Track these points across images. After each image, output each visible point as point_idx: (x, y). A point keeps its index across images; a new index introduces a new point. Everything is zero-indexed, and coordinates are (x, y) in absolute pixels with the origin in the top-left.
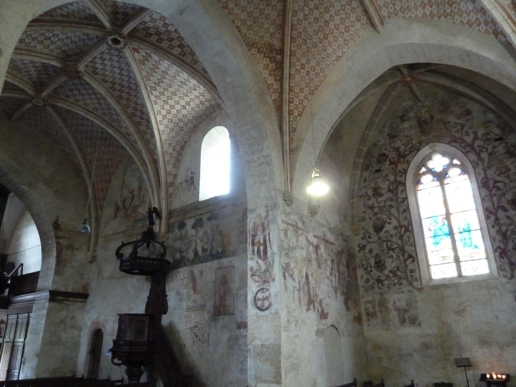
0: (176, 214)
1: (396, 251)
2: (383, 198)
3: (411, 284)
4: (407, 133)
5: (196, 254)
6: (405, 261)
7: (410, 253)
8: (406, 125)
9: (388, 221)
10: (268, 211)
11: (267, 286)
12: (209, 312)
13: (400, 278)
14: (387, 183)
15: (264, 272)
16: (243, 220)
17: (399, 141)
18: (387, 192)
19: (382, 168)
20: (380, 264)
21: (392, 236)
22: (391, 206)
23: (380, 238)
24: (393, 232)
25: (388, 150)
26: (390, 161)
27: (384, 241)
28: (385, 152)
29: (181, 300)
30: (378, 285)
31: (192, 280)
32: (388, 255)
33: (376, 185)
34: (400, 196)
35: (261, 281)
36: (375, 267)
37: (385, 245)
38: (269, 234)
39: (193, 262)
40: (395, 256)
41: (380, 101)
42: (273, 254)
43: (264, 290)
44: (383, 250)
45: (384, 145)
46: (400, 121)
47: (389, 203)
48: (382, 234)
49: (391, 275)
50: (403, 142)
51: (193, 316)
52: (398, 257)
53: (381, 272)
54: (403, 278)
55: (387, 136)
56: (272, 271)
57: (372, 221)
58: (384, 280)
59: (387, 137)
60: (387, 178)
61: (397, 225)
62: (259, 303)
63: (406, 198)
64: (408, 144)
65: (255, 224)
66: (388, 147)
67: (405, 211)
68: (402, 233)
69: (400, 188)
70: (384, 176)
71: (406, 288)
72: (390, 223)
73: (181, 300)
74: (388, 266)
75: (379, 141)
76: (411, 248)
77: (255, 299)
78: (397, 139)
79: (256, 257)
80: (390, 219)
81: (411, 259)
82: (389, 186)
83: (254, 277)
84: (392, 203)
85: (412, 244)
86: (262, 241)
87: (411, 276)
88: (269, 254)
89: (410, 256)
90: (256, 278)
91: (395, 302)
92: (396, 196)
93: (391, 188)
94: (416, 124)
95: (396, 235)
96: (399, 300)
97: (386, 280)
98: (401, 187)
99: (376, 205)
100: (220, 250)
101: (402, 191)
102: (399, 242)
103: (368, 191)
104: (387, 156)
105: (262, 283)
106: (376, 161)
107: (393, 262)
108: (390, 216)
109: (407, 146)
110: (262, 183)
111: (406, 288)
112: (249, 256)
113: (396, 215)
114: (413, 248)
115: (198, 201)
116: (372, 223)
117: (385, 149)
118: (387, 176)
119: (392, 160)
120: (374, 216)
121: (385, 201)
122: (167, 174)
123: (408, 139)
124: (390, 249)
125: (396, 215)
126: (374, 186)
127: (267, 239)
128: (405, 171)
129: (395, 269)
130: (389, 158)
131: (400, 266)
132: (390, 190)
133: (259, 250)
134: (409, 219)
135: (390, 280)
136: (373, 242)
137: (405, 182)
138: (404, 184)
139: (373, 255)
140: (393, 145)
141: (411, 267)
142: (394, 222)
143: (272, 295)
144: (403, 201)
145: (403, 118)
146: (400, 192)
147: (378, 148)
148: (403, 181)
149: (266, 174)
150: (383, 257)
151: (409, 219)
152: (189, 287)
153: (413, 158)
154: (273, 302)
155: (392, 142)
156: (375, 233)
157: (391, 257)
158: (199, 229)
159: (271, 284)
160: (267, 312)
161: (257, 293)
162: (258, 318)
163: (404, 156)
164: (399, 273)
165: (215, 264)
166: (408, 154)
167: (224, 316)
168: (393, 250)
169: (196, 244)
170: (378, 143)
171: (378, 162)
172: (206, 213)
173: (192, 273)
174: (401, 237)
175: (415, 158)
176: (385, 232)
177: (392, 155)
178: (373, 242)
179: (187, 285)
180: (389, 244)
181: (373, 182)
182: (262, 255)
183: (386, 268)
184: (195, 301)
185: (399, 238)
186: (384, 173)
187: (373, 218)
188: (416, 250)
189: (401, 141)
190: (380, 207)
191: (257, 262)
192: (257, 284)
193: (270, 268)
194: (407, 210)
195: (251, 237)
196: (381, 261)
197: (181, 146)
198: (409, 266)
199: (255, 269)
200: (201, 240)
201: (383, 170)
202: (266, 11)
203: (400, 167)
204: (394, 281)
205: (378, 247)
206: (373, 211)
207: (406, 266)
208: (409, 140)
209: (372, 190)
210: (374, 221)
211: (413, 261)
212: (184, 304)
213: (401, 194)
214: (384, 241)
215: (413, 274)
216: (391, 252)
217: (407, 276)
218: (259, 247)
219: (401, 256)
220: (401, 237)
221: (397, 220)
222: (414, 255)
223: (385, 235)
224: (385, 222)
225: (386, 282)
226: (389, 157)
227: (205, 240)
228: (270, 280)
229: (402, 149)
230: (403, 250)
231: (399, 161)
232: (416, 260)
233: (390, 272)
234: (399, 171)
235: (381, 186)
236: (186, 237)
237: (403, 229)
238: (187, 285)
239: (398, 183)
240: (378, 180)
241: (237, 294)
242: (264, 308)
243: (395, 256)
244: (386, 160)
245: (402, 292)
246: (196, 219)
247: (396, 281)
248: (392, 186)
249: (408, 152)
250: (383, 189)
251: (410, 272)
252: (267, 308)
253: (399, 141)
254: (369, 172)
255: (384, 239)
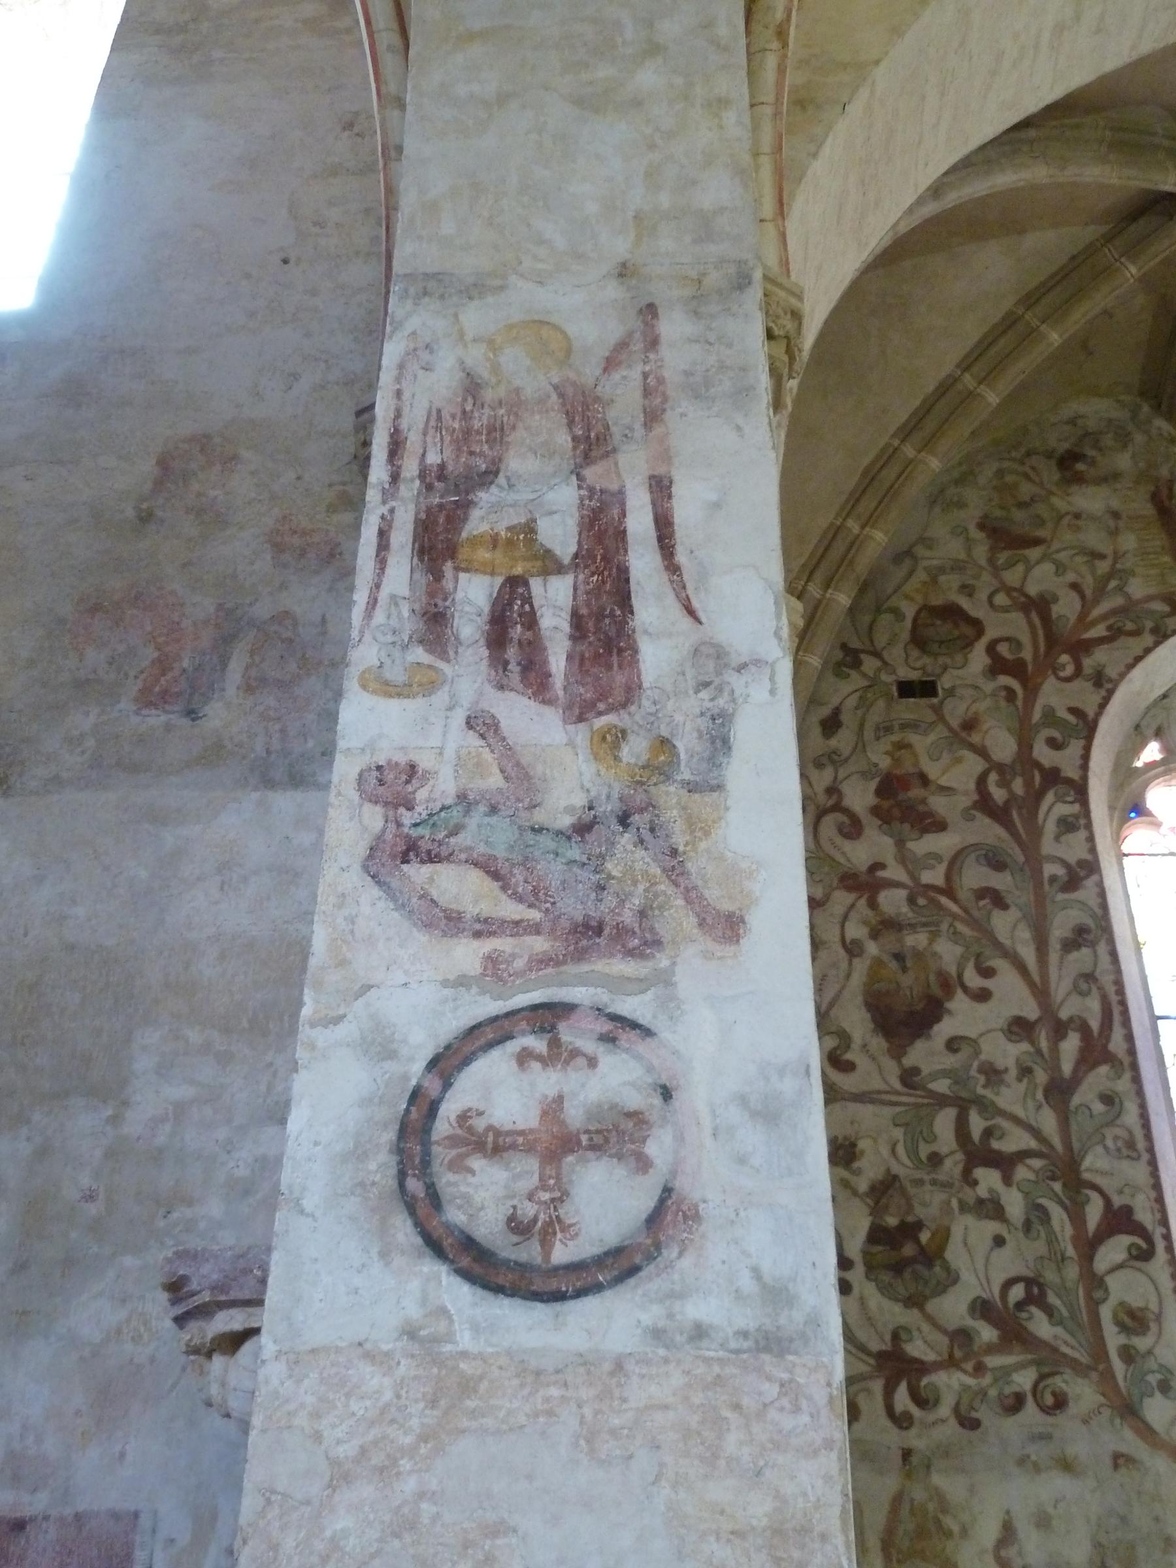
1: (1022, 1173)
2: (943, 843)
3: (1129, 1411)
4: (1094, 538)
6: (1089, 1246)
7: (1117, 1201)
8: (1091, 500)
9: (973, 979)
10: (650, 311)
11: (620, 985)
13: (1049, 1360)
14: (973, 765)
15: (583, 829)
16: (146, 518)
17: (1048, 567)
18: (967, 816)
19: (945, 682)
20: (908, 1250)
21: (993, 1074)
22: (998, 900)
23: (910, 1078)
24: (1008, 1054)
25: (983, 595)
26: (991, 649)
27: (942, 1101)
28: (964, 603)
30: (889, 1393)
32: (969, 1195)
33: (897, 761)
34: (1048, 846)
35: (518, 927)
36: (871, 1269)
37: (944, 1122)
38: (661, 488)
40: (1014, 1204)
41: (1030, 300)
42: (713, 664)
43: (577, 1034)
44: (935, 1160)
45: (958, 567)
46: (1056, 476)
47: (974, 876)
48: (927, 1054)
49: (987, 1333)
50: (1071, 577)
52: (1037, 1217)
53: (915, 1301)
54: (1074, 1364)
55: (981, 526)
56: (699, 828)
57: (861, 968)
58: (937, 1366)
59: (976, 534)
60: (975, 738)
61: (1031, 1011)
62: (484, 1196)
63: (1091, 866)
64: (1101, 592)
65: (472, 387)
66: (985, 583)
67: (1079, 938)
68: (1067, 1068)
69: (1054, 808)
70: (955, 723)
71: (1089, 1434)
72: (983, 996)
74: (966, 1276)
75: (926, 541)
76: (1125, 1165)
77: (417, 1139)
78: (1034, 553)
79: (468, 673)
80: (987, 973)
81: (1125, 1240)
82: (982, 781)
83: (418, 873)
84: (1001, 881)
85: (1131, 1144)
86: (561, 534)
87: (1128, 1355)
88: (659, 651)
89: (1120, 1220)
90: (459, 886)
91: (1008, 1533)
92: (1030, 844)
93: (998, 795)
94: (1149, 510)
95: (1025, 1072)
96: (1043, 1522)
97: (951, 1363)
98: (1060, 799)
99: (894, 872)
101: (1067, 826)
102: (1048, 1121)
103: (846, 788)
104: (978, 626)
105: (540, 944)
106: (905, 636)
107: (999, 1241)
108: (986, 952)
109: (1096, 601)
110: (591, 103)
111: (1089, 1434)
112: (365, 655)
113: (1028, 954)
114: (1138, 1172)
116: (858, 978)
117: (968, 590)
118: (970, 725)
119: (1003, 649)
120: (875, 935)
121: (956, 861)
123: (1103, 567)
124: (980, 1154)
125: (1028, 954)
126: (885, 763)
127: (639, 522)
128: (1088, 728)
129: (1017, 1292)
130: (990, 634)
131: (1050, 1275)
132: (984, 803)
133: (509, 624)
134: (1111, 990)
135: (979, 1369)
136: (861, 1098)
137: (1085, 778)
138: (1080, 791)
139: (863, 1186)
140: (1012, 577)
141: (1126, 1288)
142: (1012, 997)
143: (700, 1094)
144: (1072, 882)
145: (1070, 464)
146: (1050, 828)
147: (921, 576)
148: (1071, 771)
149: (653, 49)
150: (929, 1205)
151: (1111, 990)
153: (1131, 667)
154: (710, 1181)
155: (1010, 565)
156: (878, 1043)
157: (992, 1209)
159: (692, 964)
160: (610, 1322)
161: (448, 1062)
162: (453, 1388)
163: (1081, 648)
164: (1041, 1326)
166: (1101, 641)
168: (1005, 1164)
170: (920, 551)
171: (919, 641)
174: (1059, 1092)
175: (1137, 673)
176: (953, 1045)
177: (1007, 625)
178: (861, 1098)
180: (977, 1124)
181: (886, 743)
182: (557, 661)
183: (953, 1278)
185: (1047, 1092)
186: (955, 711)
187: (872, 948)
188: (1157, 1186)
189: (1060, 569)
190: (917, 893)
191: (482, 725)
192: (467, 954)
193: (669, 796)
194: (1096, 933)
195: (410, 489)
196: (919, 1225)
198: (1112, 1282)
199: (444, 785)
201: (951, 692)
203: (1054, 695)
204: (1005, 1373)
205: (899, 1133)
206: (873, 904)
207: (1095, 1283)
208: (1111, 575)
209: (873, 785)
210: (878, 963)
211: (1144, 1255)
213: (1057, 838)
214: (942, 1101)
215: (1141, 1343)
216: (988, 1179)
217: (1100, 1352)
218: (515, 584)
219: (1058, 1215)
220: (1059, 1092)
221: (1031, 984)
222: (1144, 1215)
223: (950, 1061)
224: (948, 985)
225: (950, 1384)
226: (990, 634)
228: (676, 918)
229: (1066, 608)
230: (1068, 1173)
231: (1048, 665)
232: (1160, 1245)
233: (982, 1308)
234: (1050, 716)
235: (932, 770)
237: (1071, 1045)
239: (1037, 778)
240: (914, 738)
242: (561, 1254)
243: (1014, 1204)
244: (969, 644)
245: (1067, 1466)
247: (1024, 1380)
248: (1004, 783)
249: (1099, 631)
250: (946, 790)
251: (1123, 1328)
252: (618, 1266)
253: (1048, 567)
254: (856, 681)
255: (942, 1086)
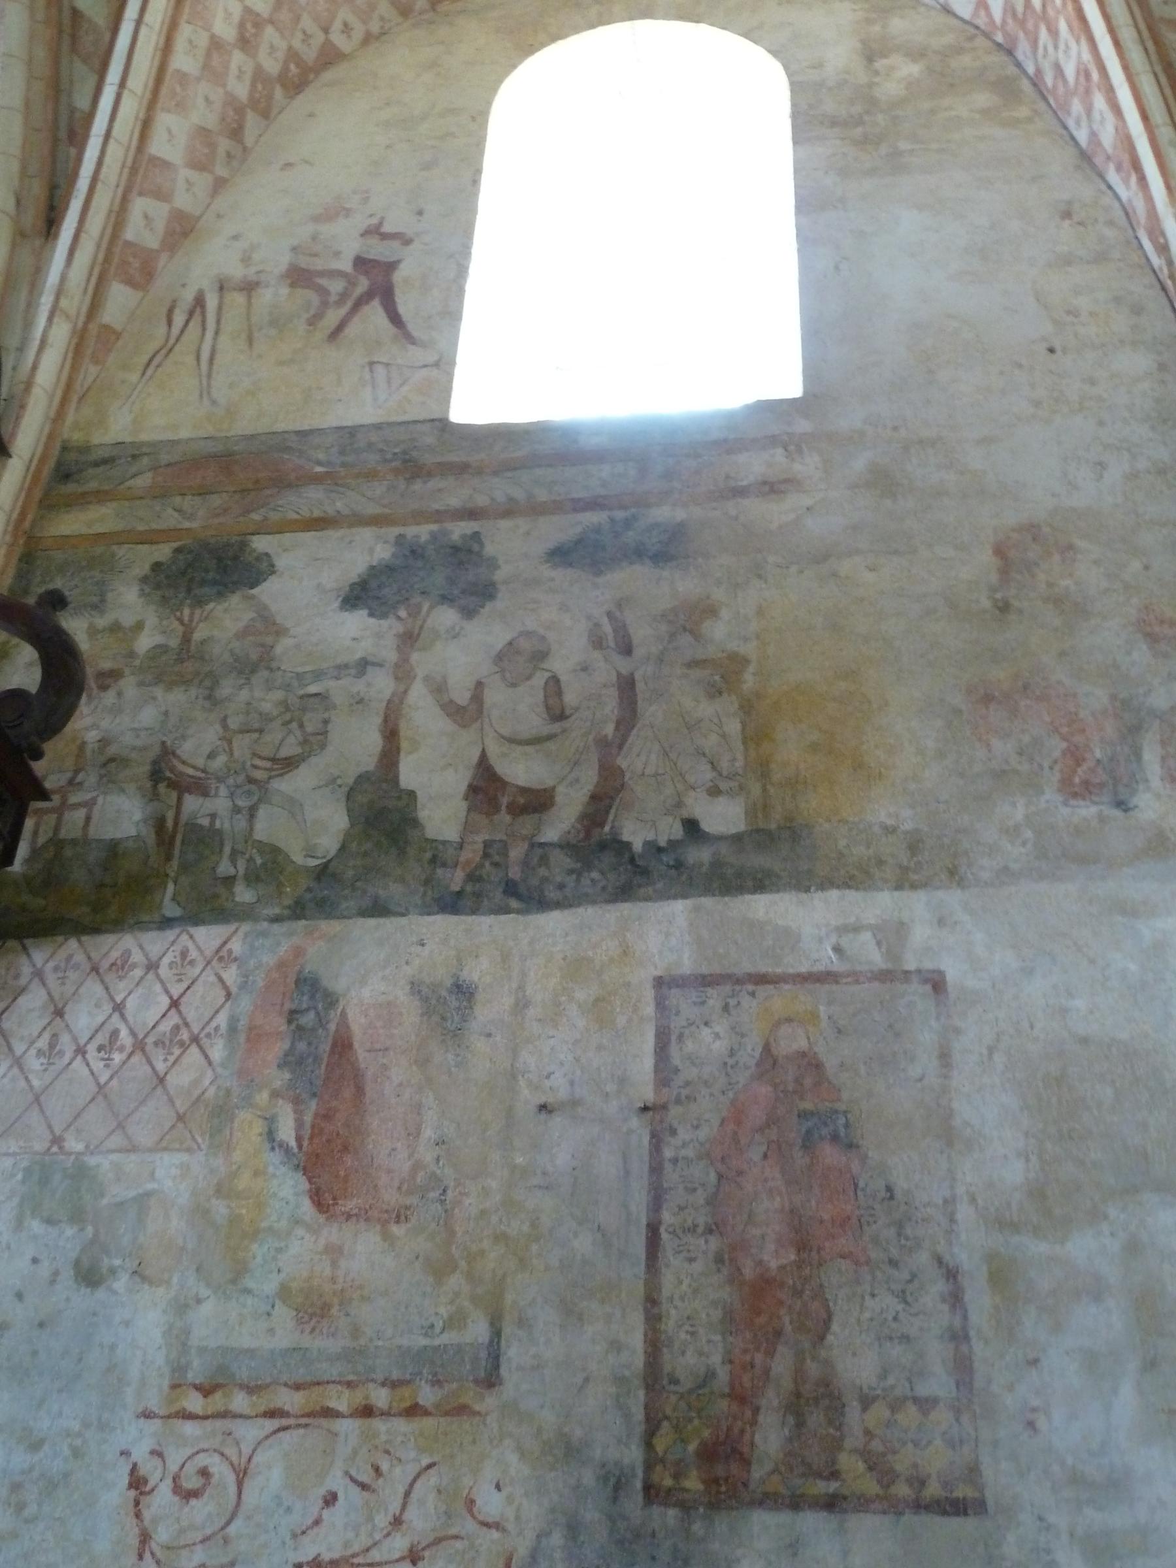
0: (143, 481)
5: (382, 815)
12: (567, 1450)
16: (1004, 608)
29: (89, 1276)
31: (292, 1062)
39: (321, 893)
51: (270, 1477)
73: (89, 1276)
100: (723, 816)
115: (443, 425)
122: (142, 170)
152: (247, 1129)
158: (446, 617)
165: (665, 932)
167: (811, 1521)
169: (391, 735)
172: (536, 510)
173: (307, 1000)
179: (221, 1114)
184: (314, 1307)
197: (292, 55)
200: (467, 712)
202: (352, 19)
212: (142, 1326)
227: (519, 708)
236: (254, 664)
238: (221, 1114)
241: (1002, 1274)
246: (400, 540)
